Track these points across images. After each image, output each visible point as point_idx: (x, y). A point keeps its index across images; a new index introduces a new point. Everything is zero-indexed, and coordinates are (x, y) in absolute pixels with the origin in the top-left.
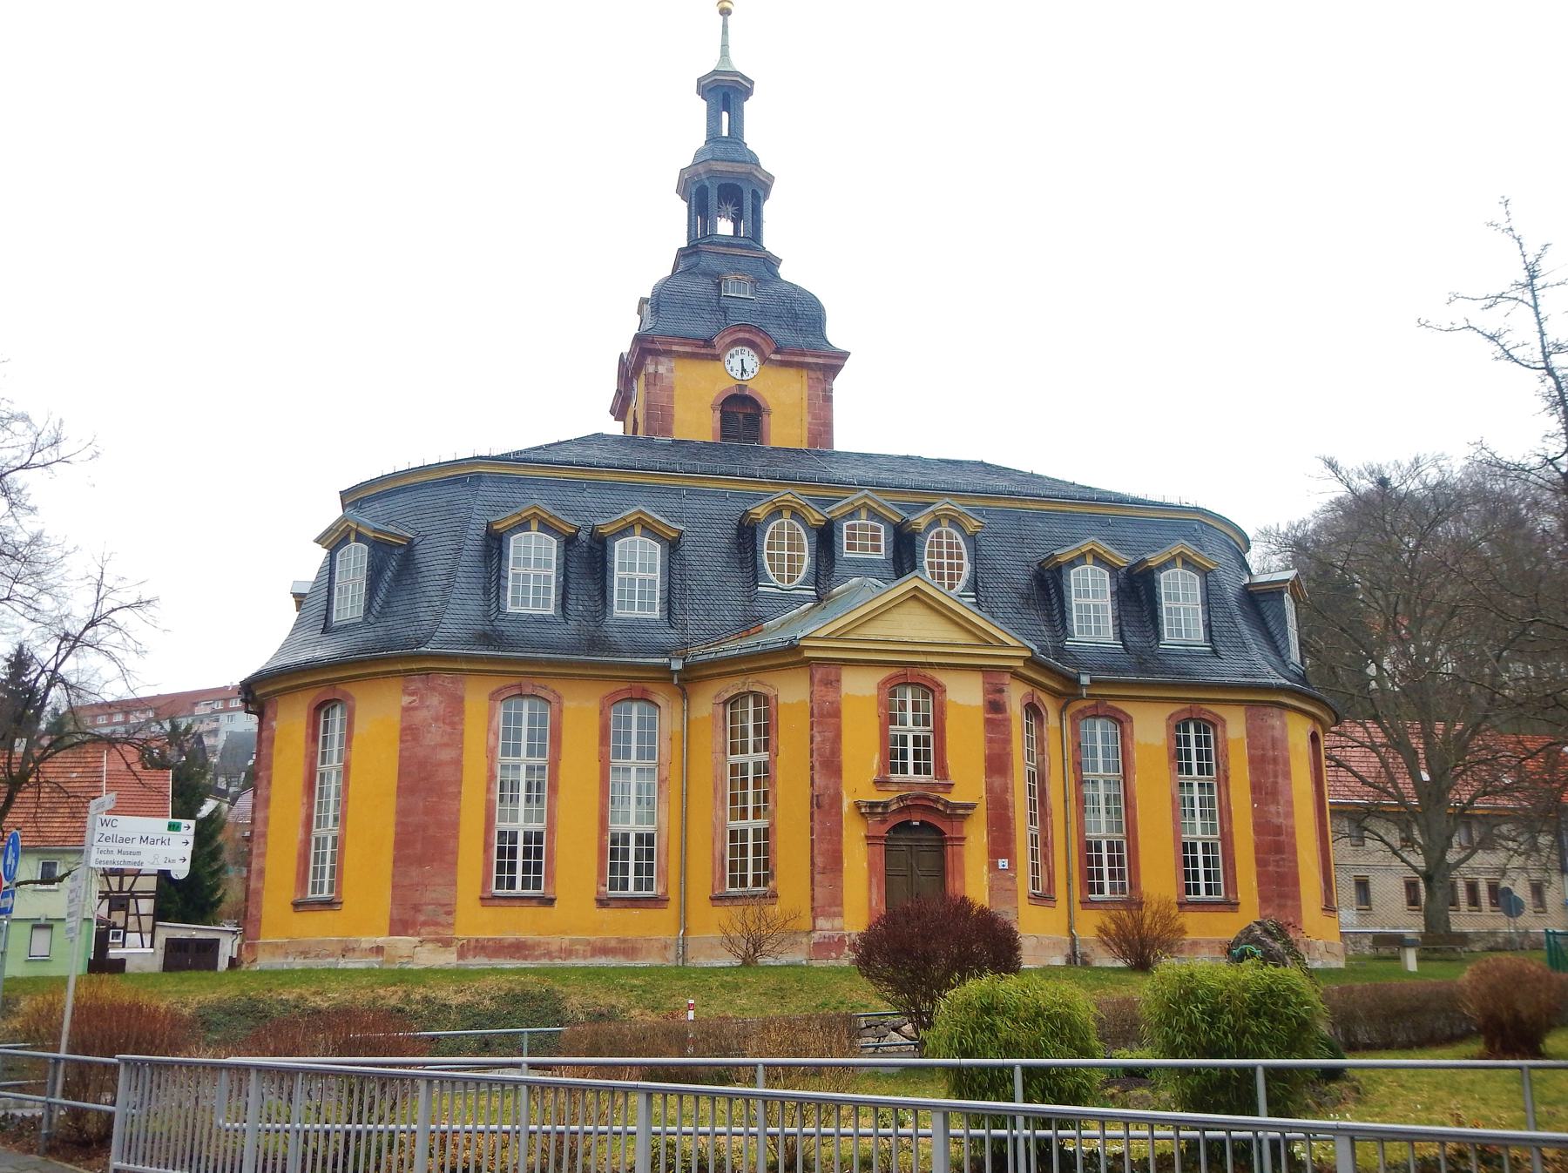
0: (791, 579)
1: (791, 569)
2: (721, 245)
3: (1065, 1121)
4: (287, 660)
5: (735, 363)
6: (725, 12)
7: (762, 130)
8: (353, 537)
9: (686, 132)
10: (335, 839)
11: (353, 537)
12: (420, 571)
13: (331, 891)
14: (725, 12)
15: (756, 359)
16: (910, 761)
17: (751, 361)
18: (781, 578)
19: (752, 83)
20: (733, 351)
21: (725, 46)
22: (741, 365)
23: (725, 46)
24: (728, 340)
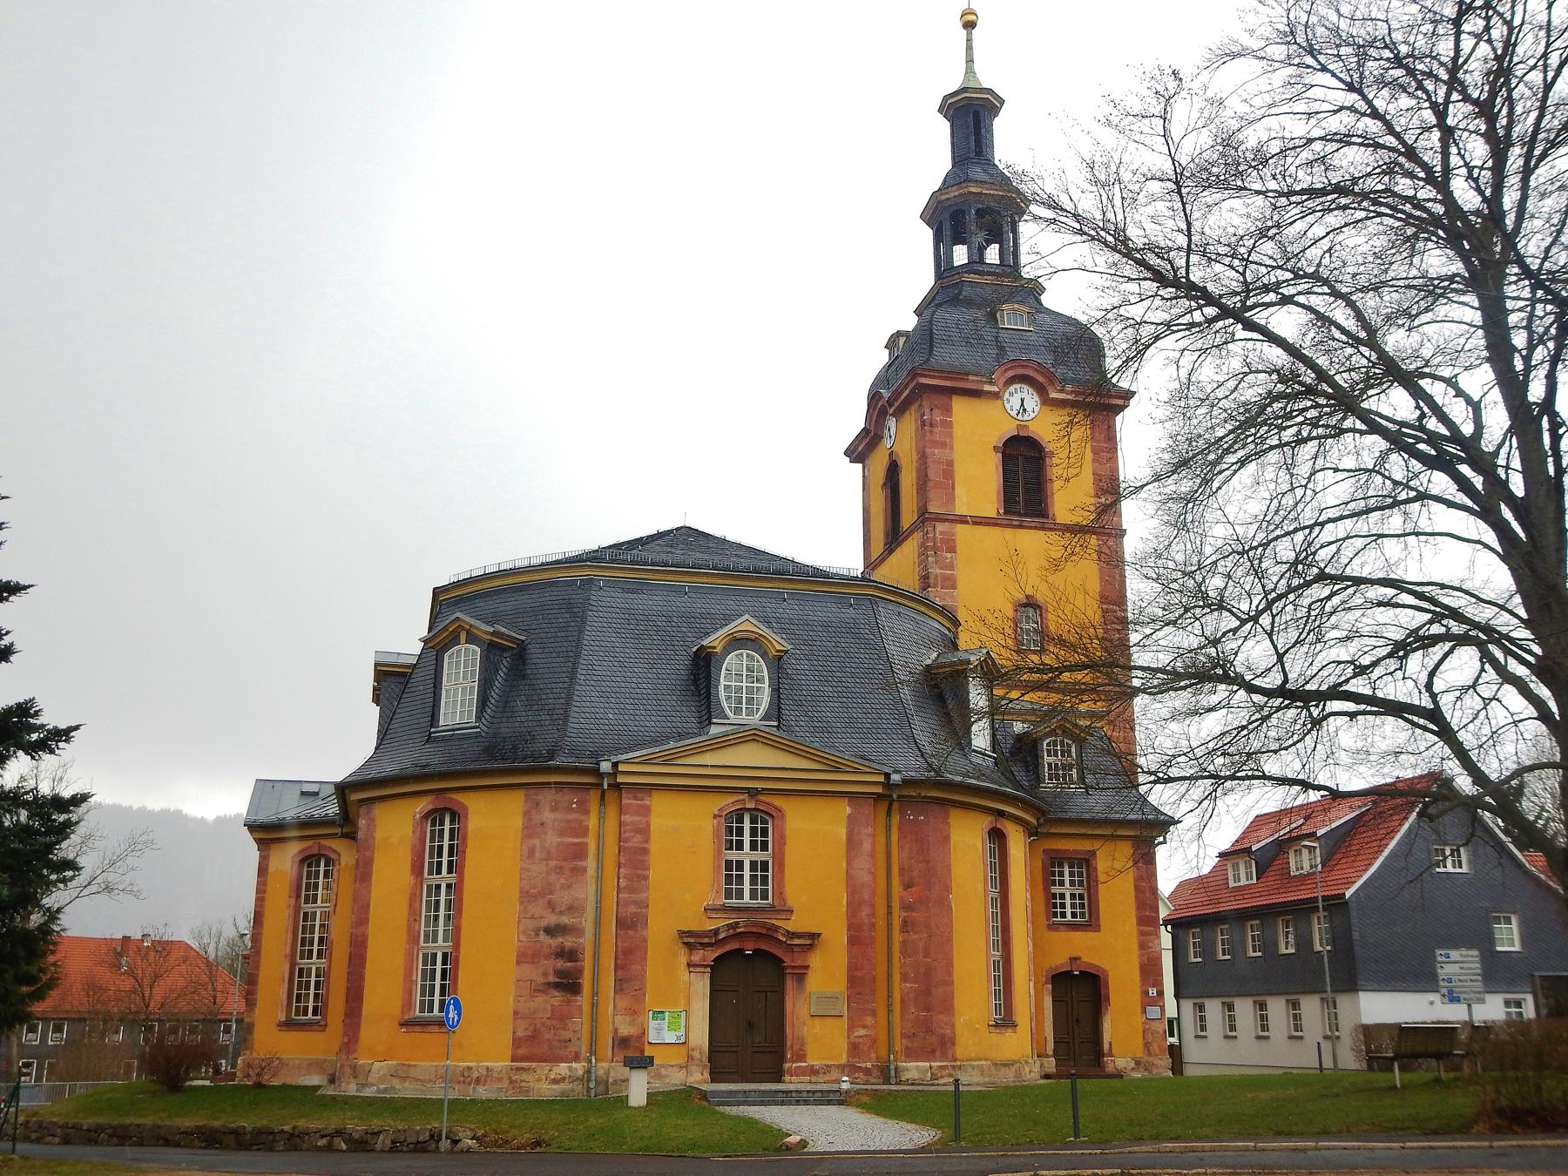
0: (750, 712)
1: (750, 701)
2: (989, 274)
3: (415, 1151)
4: (373, 774)
5: (1014, 403)
6: (970, 26)
7: (1011, 145)
8: (463, 636)
9: (932, 157)
10: (445, 955)
11: (463, 636)
12: (531, 678)
13: (441, 1010)
14: (970, 26)
15: (1036, 398)
16: (747, 873)
17: (1032, 401)
18: (738, 711)
19: (1002, 102)
20: (1012, 389)
21: (970, 60)
22: (1021, 406)
23: (970, 60)
24: (1010, 373)
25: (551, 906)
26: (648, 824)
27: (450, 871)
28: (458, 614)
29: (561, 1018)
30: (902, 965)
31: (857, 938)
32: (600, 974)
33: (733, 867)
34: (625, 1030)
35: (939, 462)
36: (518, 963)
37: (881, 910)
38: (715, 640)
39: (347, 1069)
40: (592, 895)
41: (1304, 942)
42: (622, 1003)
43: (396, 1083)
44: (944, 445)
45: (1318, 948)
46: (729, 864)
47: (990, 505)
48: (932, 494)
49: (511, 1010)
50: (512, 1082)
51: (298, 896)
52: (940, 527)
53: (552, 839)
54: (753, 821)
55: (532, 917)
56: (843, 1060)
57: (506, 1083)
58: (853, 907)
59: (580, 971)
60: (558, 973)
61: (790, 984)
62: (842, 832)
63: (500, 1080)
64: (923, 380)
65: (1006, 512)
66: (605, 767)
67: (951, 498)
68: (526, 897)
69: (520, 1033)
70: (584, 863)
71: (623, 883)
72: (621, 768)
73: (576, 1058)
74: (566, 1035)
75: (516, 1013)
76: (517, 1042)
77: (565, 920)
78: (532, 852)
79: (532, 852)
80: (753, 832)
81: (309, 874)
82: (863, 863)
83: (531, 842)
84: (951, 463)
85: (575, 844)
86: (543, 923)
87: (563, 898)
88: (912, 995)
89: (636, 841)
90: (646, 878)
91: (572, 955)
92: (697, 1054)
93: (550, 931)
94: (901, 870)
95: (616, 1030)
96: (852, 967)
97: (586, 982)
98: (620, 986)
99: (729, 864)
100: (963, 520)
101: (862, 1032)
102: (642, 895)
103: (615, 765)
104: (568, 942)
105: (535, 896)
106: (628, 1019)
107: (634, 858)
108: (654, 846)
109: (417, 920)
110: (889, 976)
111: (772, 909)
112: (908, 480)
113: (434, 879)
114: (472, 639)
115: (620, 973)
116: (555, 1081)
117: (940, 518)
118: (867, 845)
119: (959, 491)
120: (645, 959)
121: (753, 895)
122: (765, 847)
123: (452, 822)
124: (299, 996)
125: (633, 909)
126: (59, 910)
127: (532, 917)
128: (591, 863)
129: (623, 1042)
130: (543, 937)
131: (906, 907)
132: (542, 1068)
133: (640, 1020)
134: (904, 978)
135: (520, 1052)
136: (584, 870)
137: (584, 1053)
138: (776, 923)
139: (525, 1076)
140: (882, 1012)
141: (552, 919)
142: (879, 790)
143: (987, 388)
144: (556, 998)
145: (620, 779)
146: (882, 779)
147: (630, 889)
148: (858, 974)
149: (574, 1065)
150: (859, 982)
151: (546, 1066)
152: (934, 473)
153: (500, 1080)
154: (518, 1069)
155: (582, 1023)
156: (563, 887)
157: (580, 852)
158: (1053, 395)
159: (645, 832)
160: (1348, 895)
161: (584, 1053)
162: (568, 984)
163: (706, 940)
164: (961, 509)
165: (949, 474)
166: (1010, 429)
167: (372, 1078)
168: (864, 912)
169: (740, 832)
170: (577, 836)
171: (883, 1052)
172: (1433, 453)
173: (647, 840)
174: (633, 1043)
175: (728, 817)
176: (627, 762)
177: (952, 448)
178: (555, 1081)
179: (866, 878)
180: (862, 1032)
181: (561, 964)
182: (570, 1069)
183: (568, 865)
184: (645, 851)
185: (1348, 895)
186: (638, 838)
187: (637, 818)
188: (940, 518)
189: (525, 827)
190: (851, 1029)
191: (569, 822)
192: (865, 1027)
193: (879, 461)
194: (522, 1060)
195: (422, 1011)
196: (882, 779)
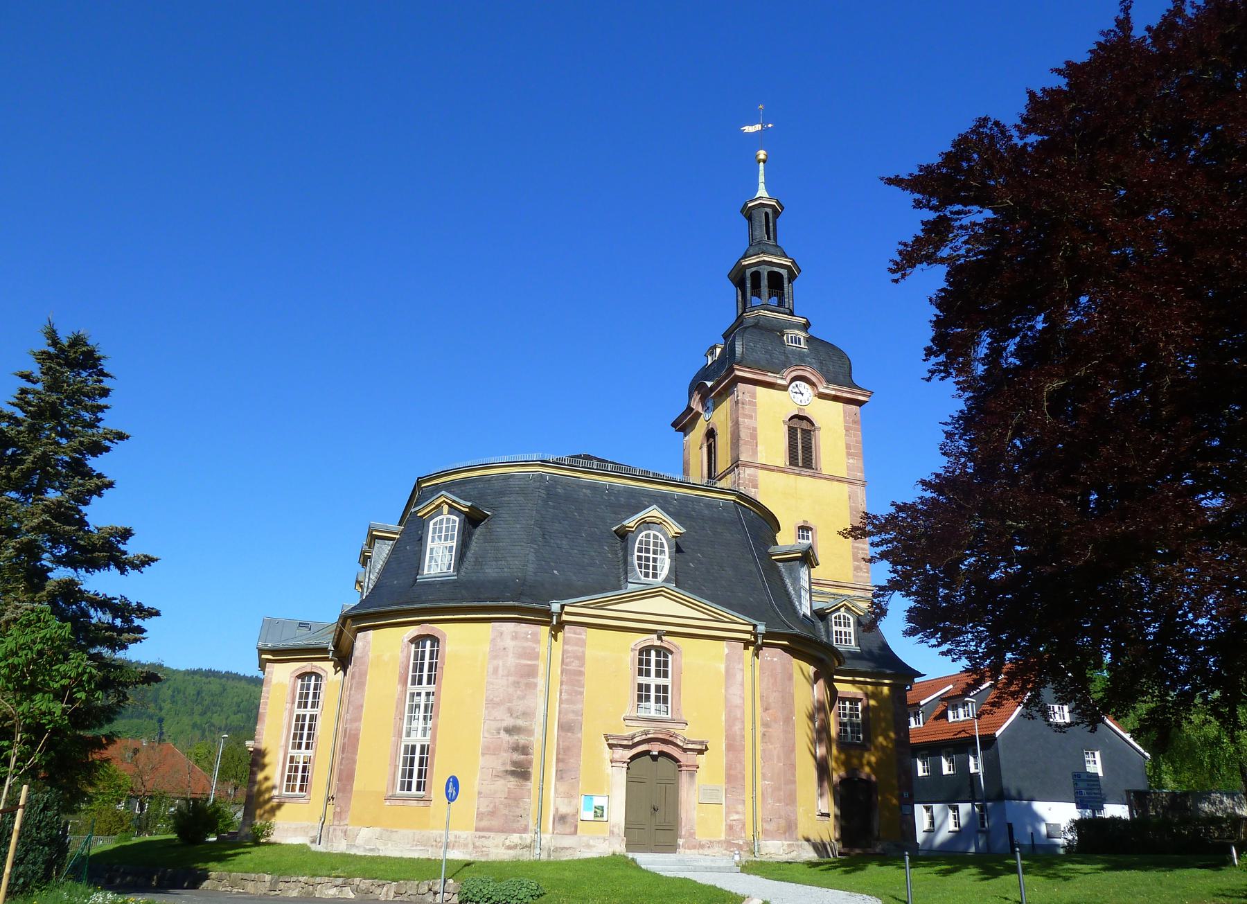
10: (423, 747)
25: (510, 712)
26: (584, 653)
27: (429, 683)
29: (514, 799)
30: (763, 767)
31: (733, 746)
32: (545, 766)
34: (563, 810)
36: (483, 754)
37: (748, 726)
38: (631, 522)
39: (339, 833)
40: (543, 707)
41: (963, 767)
42: (562, 789)
43: (379, 845)
44: (751, 417)
45: (972, 770)
46: (640, 686)
47: (781, 459)
48: (743, 448)
49: (476, 790)
50: (475, 847)
51: (293, 703)
52: (749, 471)
53: (512, 661)
54: (658, 655)
55: (495, 720)
56: (723, 837)
58: (730, 721)
59: (530, 762)
60: (514, 763)
61: (684, 778)
62: (722, 667)
63: (466, 845)
64: (738, 373)
66: (555, 607)
67: (755, 452)
68: (492, 704)
69: (482, 810)
71: (564, 696)
72: (567, 609)
73: (525, 830)
74: (519, 812)
75: (480, 793)
76: (480, 816)
77: (520, 723)
78: (496, 670)
79: (496, 670)
80: (658, 663)
81: (302, 686)
82: (735, 690)
83: (495, 662)
84: (755, 429)
86: (505, 724)
87: (520, 706)
89: (574, 665)
90: (581, 693)
91: (524, 750)
92: (616, 830)
93: (508, 731)
94: (762, 697)
95: (557, 809)
96: (729, 767)
97: (535, 771)
98: (560, 775)
99: (640, 686)
100: (764, 467)
101: (736, 817)
102: (578, 707)
103: (563, 607)
104: (522, 739)
105: (498, 704)
106: (566, 800)
107: (573, 676)
108: (588, 669)
109: (401, 719)
110: (754, 775)
111: (672, 721)
112: (723, 441)
113: (416, 689)
115: (561, 765)
116: (509, 848)
117: (748, 465)
118: (739, 677)
119: (760, 448)
120: (579, 755)
122: (666, 675)
123: (432, 646)
124: (289, 777)
125: (571, 716)
126: (912, 184)
128: (541, 681)
129: (561, 819)
130: (503, 735)
131: (765, 724)
132: (500, 838)
134: (764, 777)
135: (484, 823)
136: (535, 685)
137: (532, 827)
139: (486, 842)
140: (749, 802)
141: (509, 722)
142: (748, 636)
143: (779, 382)
144: (512, 782)
145: (565, 617)
146: (750, 628)
147: (569, 702)
148: (732, 772)
150: (733, 778)
151: (503, 836)
152: (744, 434)
153: (466, 845)
155: (532, 804)
156: (520, 698)
157: (532, 672)
158: (822, 390)
159: (581, 658)
160: (998, 733)
161: (532, 827)
162: (521, 772)
163: (625, 743)
164: (762, 459)
165: (754, 436)
167: (359, 841)
168: (737, 727)
169: (648, 663)
170: (530, 659)
171: (749, 832)
172: (25, 787)
173: (583, 665)
174: (570, 820)
175: (641, 653)
176: (571, 605)
178: (509, 848)
179: (738, 701)
180: (736, 817)
181: (517, 757)
182: (521, 838)
183: (523, 681)
184: (581, 673)
185: (998, 733)
186: (577, 663)
187: (576, 648)
188: (748, 465)
190: (727, 814)
191: (524, 648)
192: (737, 813)
194: (483, 830)
195: (402, 789)
196: (750, 628)
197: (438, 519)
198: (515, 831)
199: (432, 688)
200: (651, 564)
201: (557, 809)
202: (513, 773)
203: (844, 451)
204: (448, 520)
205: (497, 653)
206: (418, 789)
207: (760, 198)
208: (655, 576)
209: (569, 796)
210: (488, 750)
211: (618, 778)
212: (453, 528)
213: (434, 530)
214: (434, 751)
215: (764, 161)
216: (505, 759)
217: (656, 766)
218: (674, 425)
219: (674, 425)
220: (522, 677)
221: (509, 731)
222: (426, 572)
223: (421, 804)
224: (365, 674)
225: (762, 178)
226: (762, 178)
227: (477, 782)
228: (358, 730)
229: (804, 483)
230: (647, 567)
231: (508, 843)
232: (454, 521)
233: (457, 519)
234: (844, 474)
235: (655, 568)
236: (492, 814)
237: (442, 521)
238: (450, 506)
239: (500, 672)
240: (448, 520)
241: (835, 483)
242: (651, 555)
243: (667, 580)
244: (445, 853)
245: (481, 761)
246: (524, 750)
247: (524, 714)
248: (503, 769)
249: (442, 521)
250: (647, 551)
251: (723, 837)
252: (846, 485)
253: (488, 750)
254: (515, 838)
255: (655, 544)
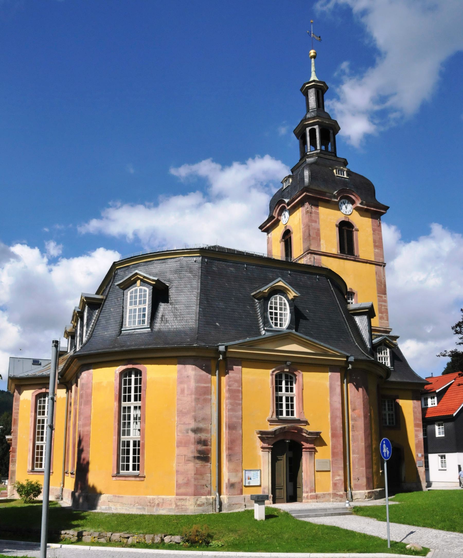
18: (276, 324)
28: (137, 271)
33: (279, 399)
34: (233, 480)
35: (314, 229)
36: (178, 446)
44: (316, 222)
47: (335, 249)
49: (175, 469)
50: (177, 506)
55: (184, 424)
57: (174, 506)
59: (209, 451)
60: (199, 452)
62: (328, 383)
65: (341, 252)
67: (319, 245)
68: (181, 413)
69: (180, 481)
70: (209, 397)
73: (210, 493)
74: (204, 482)
75: (177, 471)
77: (201, 425)
79: (183, 391)
84: (318, 230)
85: (204, 387)
88: (357, 460)
91: (205, 443)
97: (214, 456)
98: (230, 457)
103: (226, 347)
104: (203, 436)
106: (234, 474)
107: (236, 394)
114: (144, 282)
116: (199, 505)
119: (322, 242)
121: (288, 414)
125: (234, 420)
127: (184, 424)
133: (240, 474)
135: (182, 490)
138: (302, 427)
139: (183, 503)
144: (199, 463)
148: (336, 451)
149: (208, 497)
154: (180, 499)
162: (203, 457)
164: (323, 249)
165: (318, 234)
166: (342, 218)
174: (237, 486)
177: (319, 223)
178: (199, 505)
181: (200, 447)
183: (202, 397)
186: (236, 384)
189: (179, 378)
190: (333, 476)
193: (278, 232)
197: (134, 289)
198: (202, 495)
199: (138, 403)
200: (278, 317)
201: (229, 480)
202: (198, 458)
203: (372, 244)
204: (141, 290)
205: (181, 380)
206: (134, 469)
207: (314, 81)
208: (281, 325)
209: (236, 471)
210: (180, 444)
211: (265, 459)
212: (145, 295)
213: (131, 298)
214: (144, 444)
215: (314, 57)
216: (191, 450)
217: (288, 447)
218: (261, 228)
219: (261, 228)
220: (200, 395)
221: (196, 431)
222: (127, 325)
223: (138, 479)
224: (91, 395)
225: (313, 69)
226: (313, 69)
227: (174, 465)
228: (89, 432)
229: (349, 265)
230: (276, 319)
231: (198, 503)
232: (145, 291)
233: (147, 289)
234: (372, 259)
235: (281, 320)
236: (187, 484)
237: (136, 291)
238: (142, 280)
239: (186, 392)
240: (141, 290)
241: (368, 264)
242: (278, 311)
243: (289, 328)
244: (157, 510)
245: (176, 451)
246: (205, 443)
247: (203, 419)
248: (193, 455)
249: (136, 291)
250: (276, 309)
251: (331, 491)
252: (374, 266)
253: (180, 444)
254: (203, 499)
255: (281, 304)
